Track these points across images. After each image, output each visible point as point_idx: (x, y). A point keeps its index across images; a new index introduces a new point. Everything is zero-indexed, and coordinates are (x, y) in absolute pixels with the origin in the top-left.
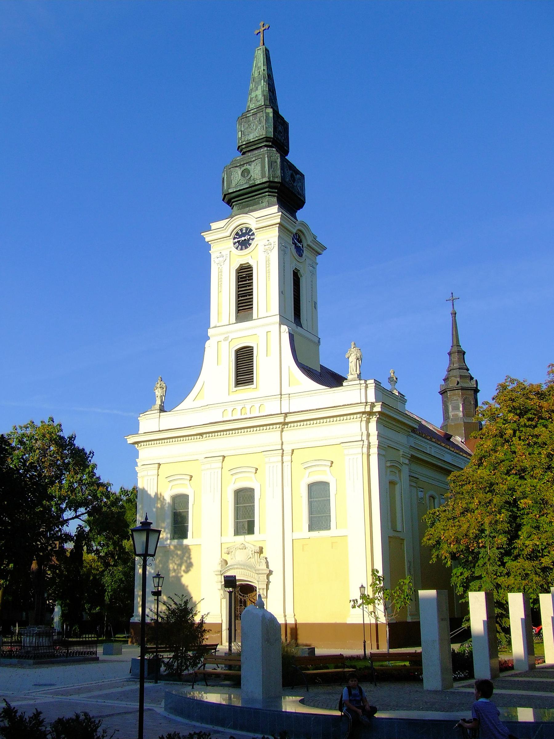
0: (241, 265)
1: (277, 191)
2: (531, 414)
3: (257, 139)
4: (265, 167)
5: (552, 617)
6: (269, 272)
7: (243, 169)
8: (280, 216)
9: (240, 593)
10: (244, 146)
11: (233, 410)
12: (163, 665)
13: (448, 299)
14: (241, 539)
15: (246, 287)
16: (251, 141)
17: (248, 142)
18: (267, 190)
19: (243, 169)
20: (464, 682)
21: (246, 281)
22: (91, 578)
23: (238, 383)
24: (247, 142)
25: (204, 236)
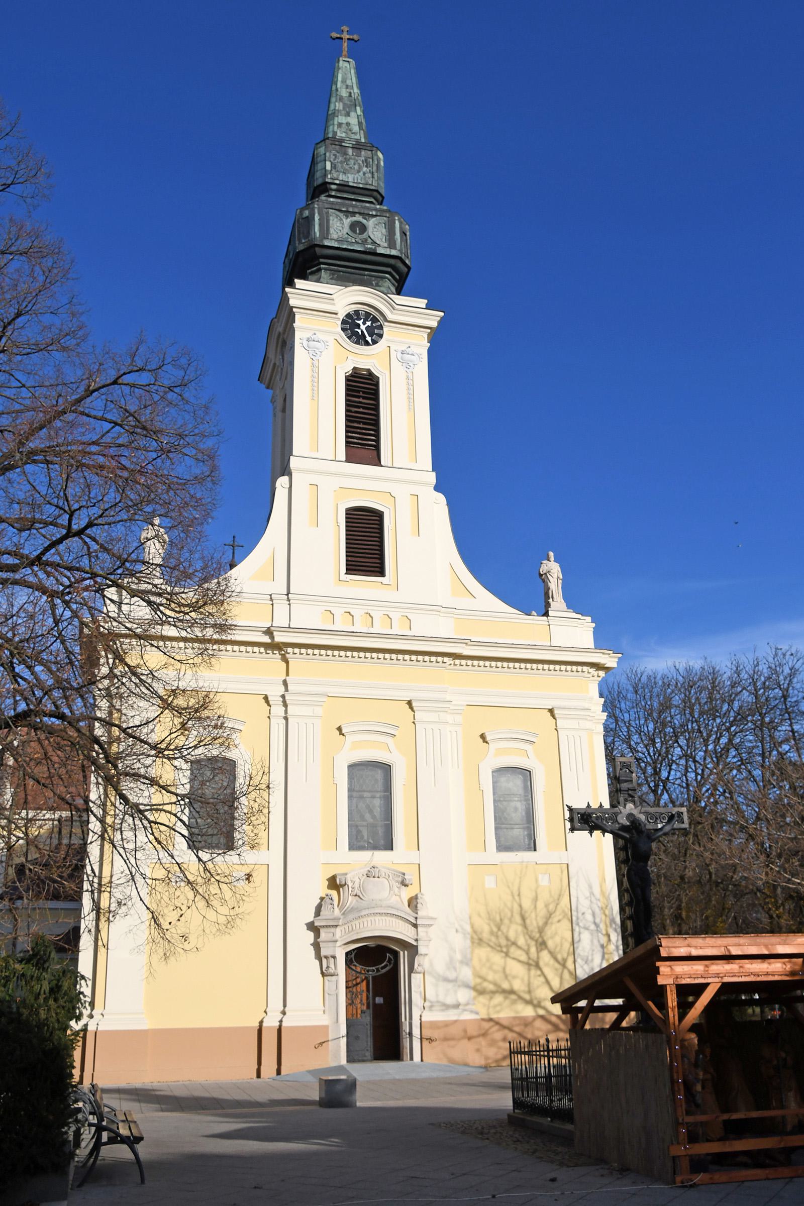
0: (355, 368)
1: (398, 277)
2: (19, 684)
3: (361, 186)
4: (395, 234)
5: (659, 974)
6: (409, 398)
7: (354, 219)
8: (439, 319)
9: (381, 966)
10: (334, 187)
11: (370, 616)
12: (76, 1106)
13: (236, 539)
14: (365, 857)
15: (359, 407)
16: (351, 184)
17: (345, 183)
18: (389, 269)
19: (354, 219)
20: (369, 1044)
21: (359, 397)
22: (641, 1025)
23: (353, 567)
24: (342, 182)
25: (289, 295)
